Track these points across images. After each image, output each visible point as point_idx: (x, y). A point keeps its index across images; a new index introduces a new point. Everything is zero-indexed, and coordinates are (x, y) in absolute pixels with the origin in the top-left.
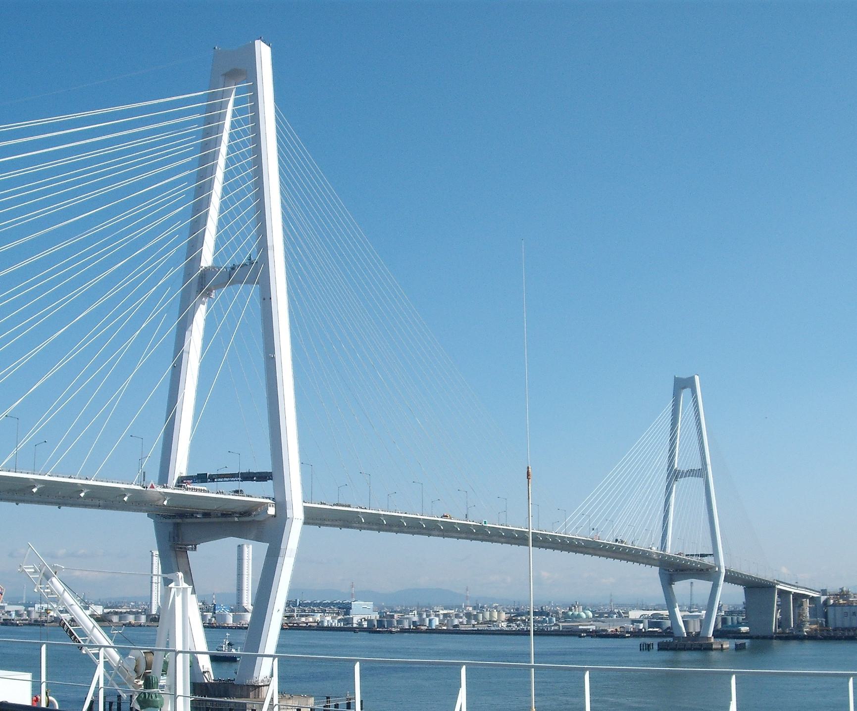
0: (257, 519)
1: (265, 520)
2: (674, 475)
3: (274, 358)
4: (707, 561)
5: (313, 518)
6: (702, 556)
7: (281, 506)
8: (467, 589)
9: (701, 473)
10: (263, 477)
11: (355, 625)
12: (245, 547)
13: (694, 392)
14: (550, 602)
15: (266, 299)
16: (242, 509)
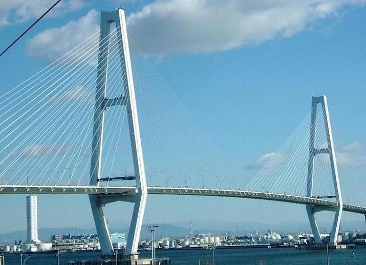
0: (132, 194)
1: (133, 195)
2: (314, 152)
3: (134, 135)
4: (333, 201)
5: (150, 192)
6: (318, 198)
7: (140, 190)
8: (191, 223)
9: (328, 151)
10: (131, 178)
11: (119, 248)
12: (32, 197)
13: (323, 105)
14: (255, 232)
15: (129, 112)
16: (126, 191)
